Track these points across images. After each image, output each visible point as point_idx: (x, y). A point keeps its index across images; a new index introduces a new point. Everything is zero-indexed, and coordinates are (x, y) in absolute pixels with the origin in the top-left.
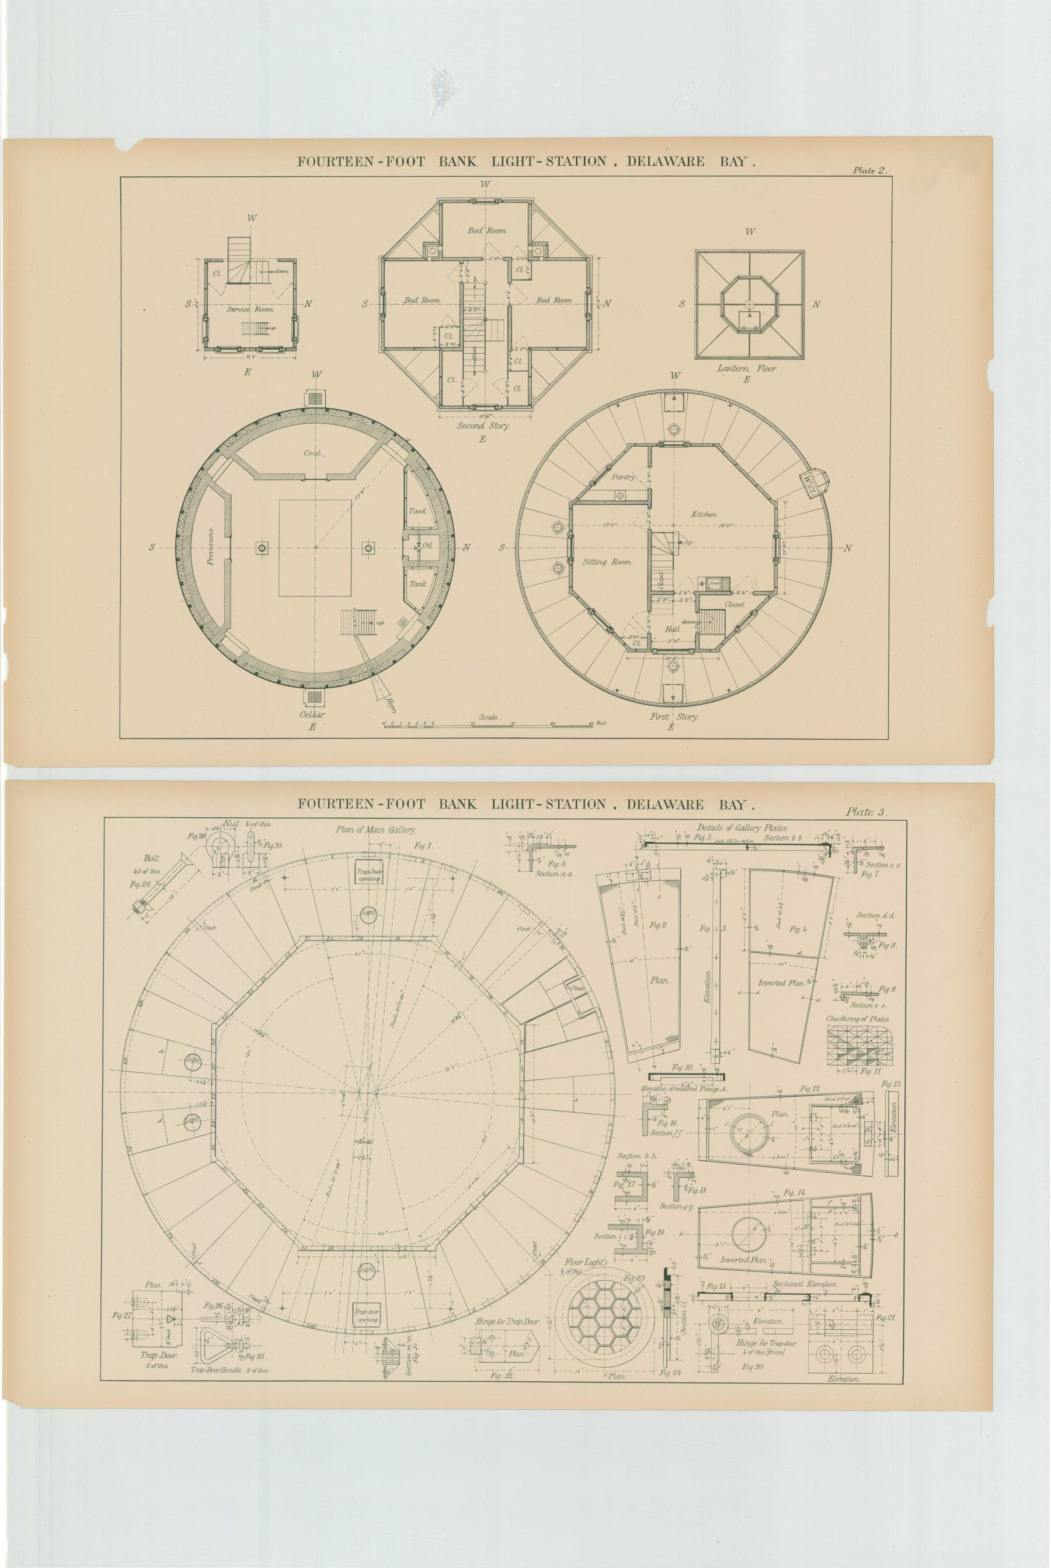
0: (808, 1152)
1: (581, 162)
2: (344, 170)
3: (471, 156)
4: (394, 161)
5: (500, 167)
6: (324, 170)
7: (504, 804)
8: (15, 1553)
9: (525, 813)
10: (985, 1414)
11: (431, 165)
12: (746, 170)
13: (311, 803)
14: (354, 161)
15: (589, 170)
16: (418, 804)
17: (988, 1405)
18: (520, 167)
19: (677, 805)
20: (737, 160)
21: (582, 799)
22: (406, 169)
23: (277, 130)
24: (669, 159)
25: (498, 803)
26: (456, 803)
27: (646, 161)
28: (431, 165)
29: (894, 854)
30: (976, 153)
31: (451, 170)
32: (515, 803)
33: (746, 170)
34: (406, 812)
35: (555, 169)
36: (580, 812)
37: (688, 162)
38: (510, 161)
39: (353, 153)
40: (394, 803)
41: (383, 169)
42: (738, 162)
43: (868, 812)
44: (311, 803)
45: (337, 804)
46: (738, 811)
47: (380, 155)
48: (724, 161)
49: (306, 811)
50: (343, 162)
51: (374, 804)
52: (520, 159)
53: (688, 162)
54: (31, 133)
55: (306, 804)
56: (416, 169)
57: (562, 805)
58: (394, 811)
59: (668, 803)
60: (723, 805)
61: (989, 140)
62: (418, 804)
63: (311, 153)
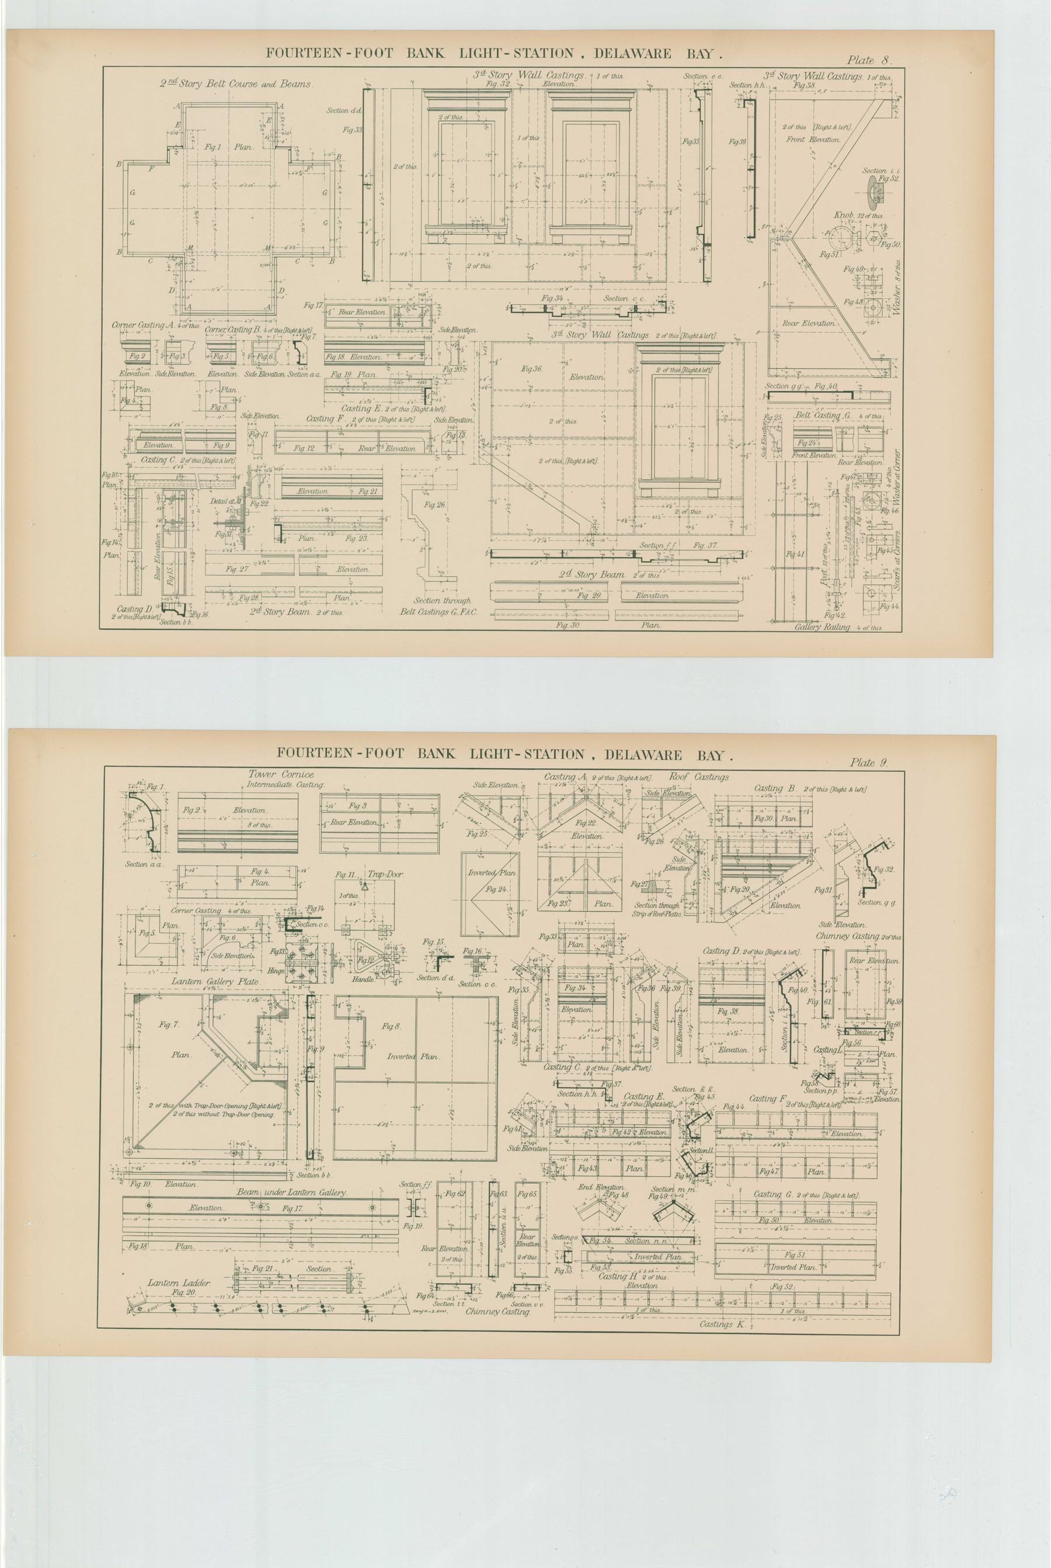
1: (548, 53)
2: (312, 61)
3: (450, 748)
4: (373, 753)
5: (479, 760)
6: (293, 61)
10: (982, 1366)
11: (410, 758)
12: (714, 61)
14: (333, 752)
16: (396, 753)
18: (499, 759)
19: (655, 755)
21: (560, 748)
22: (384, 761)
24: (636, 51)
25: (466, 52)
26: (424, 52)
27: (624, 754)
28: (399, 57)
30: (985, 746)
31: (420, 61)
32: (483, 52)
33: (714, 61)
37: (655, 54)
38: (478, 52)
39: (321, 45)
40: (362, 52)
41: (351, 60)
42: (705, 54)
45: (305, 53)
46: (716, 762)
47: (358, 747)
48: (690, 54)
49: (274, 60)
50: (323, 753)
51: (353, 752)
52: (498, 752)
53: (655, 54)
55: (285, 752)
56: (384, 61)
59: (636, 51)
60: (701, 756)
62: (386, 53)
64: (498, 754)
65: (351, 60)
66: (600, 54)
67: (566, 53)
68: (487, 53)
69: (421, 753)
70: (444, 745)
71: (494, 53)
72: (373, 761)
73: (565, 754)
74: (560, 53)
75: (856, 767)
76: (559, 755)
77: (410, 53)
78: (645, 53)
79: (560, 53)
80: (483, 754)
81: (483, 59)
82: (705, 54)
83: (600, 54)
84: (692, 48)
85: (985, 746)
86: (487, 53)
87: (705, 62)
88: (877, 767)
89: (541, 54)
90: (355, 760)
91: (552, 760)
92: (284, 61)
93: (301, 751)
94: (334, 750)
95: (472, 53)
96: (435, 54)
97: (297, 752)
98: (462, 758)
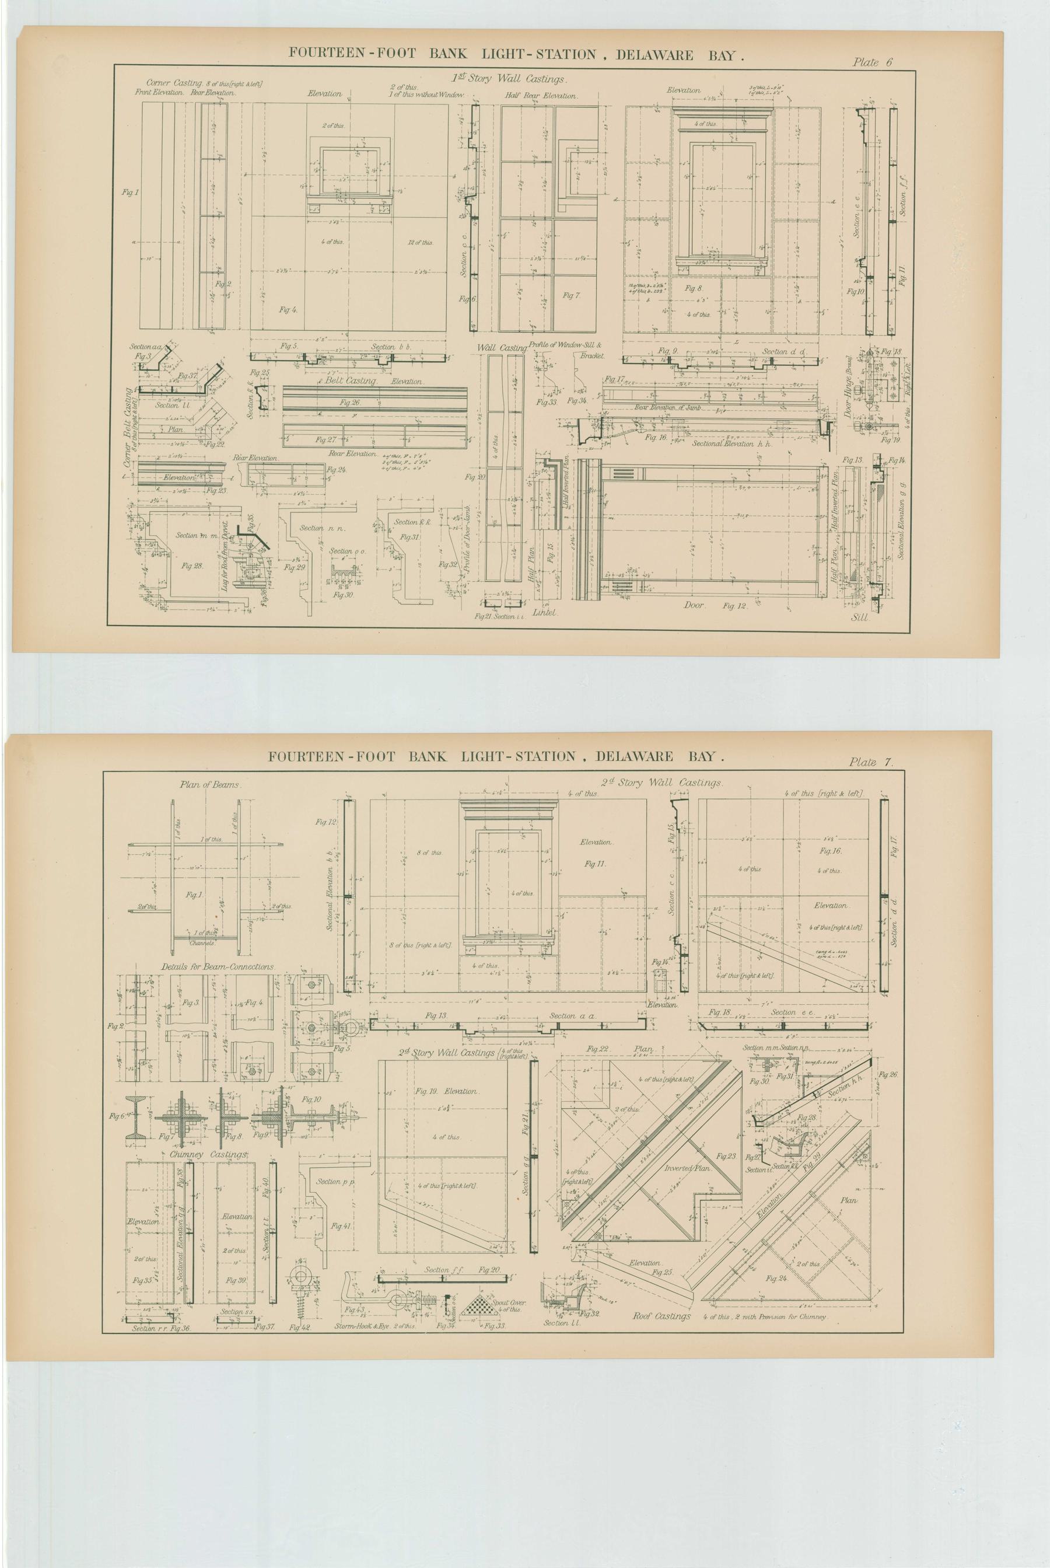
0: (795, 218)
2: (314, 765)
4: (385, 53)
9: (494, 765)
13: (282, 756)
14: (324, 756)
15: (579, 63)
16: (388, 757)
17: (989, 1351)
18: (490, 762)
20: (726, 54)
23: (276, 21)
24: (658, 53)
25: (468, 756)
26: (447, 52)
27: (635, 54)
29: (876, 622)
30: (981, 742)
31: (421, 765)
33: (736, 63)
35: (524, 764)
36: (550, 764)
37: (677, 56)
38: (480, 756)
39: (324, 748)
40: (364, 756)
42: (727, 56)
43: (874, 62)
44: (282, 756)
45: (328, 53)
48: (712, 56)
49: (297, 59)
50: (314, 757)
53: (677, 56)
55: (276, 757)
56: (386, 765)
57: (552, 55)
59: (658, 53)
63: (281, 748)
64: (489, 757)
65: (374, 60)
66: (601, 757)
67: (568, 756)
68: (510, 54)
70: (435, 749)
71: (496, 757)
77: (434, 53)
78: (667, 55)
80: (474, 756)
82: (727, 56)
83: (601, 757)
85: (981, 742)
86: (510, 54)
87: (707, 765)
89: (542, 757)
93: (313, 50)
94: (325, 755)
95: (495, 54)
96: (457, 55)
97: (288, 756)
98: (453, 761)
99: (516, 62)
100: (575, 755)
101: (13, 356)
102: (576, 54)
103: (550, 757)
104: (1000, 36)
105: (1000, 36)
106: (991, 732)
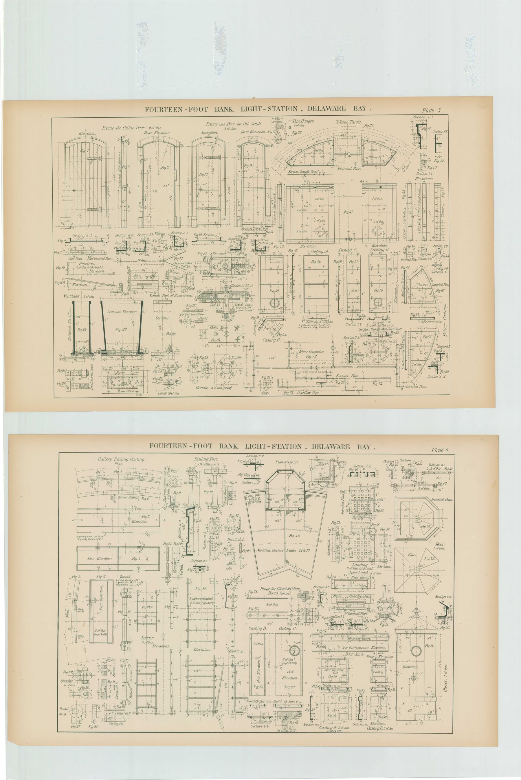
2: (173, 450)
3: (231, 106)
5: (245, 112)
6: (158, 114)
7: (247, 109)
8: (8, 775)
10: (497, 748)
11: (211, 111)
14: (173, 109)
15: (293, 451)
16: (209, 446)
17: (494, 406)
19: (337, 447)
20: (362, 107)
22: (199, 113)
24: (328, 107)
25: (248, 446)
26: (223, 108)
27: (321, 446)
30: (486, 103)
31: (221, 113)
32: (252, 108)
34: (203, 450)
37: (341, 447)
38: (254, 446)
40: (193, 109)
41: (187, 113)
42: (367, 447)
43: (432, 110)
45: (164, 110)
47: (186, 107)
48: (359, 447)
50: (168, 110)
54: (16, 432)
56: (203, 113)
57: (276, 109)
58: (197, 450)
61: (491, 98)
62: (204, 109)
64: (254, 109)
65: (187, 113)
66: (314, 447)
67: (294, 109)
69: (217, 109)
71: (262, 447)
72: (192, 113)
73: (288, 109)
74: (290, 109)
75: (434, 452)
76: (289, 447)
78: (333, 108)
79: (290, 109)
81: (252, 112)
82: (367, 447)
83: (314, 447)
84: (356, 105)
85: (486, 103)
88: (445, 452)
89: (285, 447)
90: (188, 450)
91: (281, 112)
92: (154, 114)
93: (157, 109)
94: (178, 445)
96: (229, 110)
97: (159, 446)
98: (237, 111)
99: (262, 451)
100: (297, 108)
101: (7, 539)
102: (292, 446)
103: (285, 109)
104: (497, 437)
105: (497, 437)
106: (491, 98)
